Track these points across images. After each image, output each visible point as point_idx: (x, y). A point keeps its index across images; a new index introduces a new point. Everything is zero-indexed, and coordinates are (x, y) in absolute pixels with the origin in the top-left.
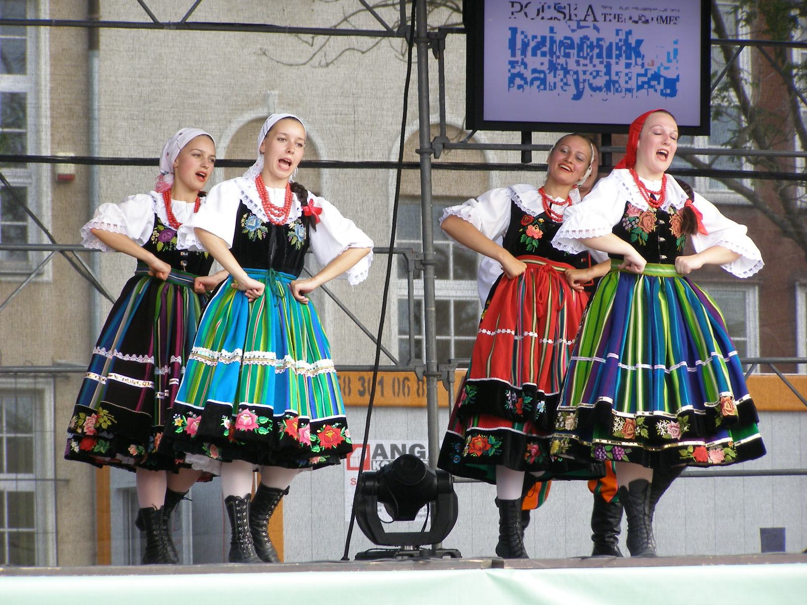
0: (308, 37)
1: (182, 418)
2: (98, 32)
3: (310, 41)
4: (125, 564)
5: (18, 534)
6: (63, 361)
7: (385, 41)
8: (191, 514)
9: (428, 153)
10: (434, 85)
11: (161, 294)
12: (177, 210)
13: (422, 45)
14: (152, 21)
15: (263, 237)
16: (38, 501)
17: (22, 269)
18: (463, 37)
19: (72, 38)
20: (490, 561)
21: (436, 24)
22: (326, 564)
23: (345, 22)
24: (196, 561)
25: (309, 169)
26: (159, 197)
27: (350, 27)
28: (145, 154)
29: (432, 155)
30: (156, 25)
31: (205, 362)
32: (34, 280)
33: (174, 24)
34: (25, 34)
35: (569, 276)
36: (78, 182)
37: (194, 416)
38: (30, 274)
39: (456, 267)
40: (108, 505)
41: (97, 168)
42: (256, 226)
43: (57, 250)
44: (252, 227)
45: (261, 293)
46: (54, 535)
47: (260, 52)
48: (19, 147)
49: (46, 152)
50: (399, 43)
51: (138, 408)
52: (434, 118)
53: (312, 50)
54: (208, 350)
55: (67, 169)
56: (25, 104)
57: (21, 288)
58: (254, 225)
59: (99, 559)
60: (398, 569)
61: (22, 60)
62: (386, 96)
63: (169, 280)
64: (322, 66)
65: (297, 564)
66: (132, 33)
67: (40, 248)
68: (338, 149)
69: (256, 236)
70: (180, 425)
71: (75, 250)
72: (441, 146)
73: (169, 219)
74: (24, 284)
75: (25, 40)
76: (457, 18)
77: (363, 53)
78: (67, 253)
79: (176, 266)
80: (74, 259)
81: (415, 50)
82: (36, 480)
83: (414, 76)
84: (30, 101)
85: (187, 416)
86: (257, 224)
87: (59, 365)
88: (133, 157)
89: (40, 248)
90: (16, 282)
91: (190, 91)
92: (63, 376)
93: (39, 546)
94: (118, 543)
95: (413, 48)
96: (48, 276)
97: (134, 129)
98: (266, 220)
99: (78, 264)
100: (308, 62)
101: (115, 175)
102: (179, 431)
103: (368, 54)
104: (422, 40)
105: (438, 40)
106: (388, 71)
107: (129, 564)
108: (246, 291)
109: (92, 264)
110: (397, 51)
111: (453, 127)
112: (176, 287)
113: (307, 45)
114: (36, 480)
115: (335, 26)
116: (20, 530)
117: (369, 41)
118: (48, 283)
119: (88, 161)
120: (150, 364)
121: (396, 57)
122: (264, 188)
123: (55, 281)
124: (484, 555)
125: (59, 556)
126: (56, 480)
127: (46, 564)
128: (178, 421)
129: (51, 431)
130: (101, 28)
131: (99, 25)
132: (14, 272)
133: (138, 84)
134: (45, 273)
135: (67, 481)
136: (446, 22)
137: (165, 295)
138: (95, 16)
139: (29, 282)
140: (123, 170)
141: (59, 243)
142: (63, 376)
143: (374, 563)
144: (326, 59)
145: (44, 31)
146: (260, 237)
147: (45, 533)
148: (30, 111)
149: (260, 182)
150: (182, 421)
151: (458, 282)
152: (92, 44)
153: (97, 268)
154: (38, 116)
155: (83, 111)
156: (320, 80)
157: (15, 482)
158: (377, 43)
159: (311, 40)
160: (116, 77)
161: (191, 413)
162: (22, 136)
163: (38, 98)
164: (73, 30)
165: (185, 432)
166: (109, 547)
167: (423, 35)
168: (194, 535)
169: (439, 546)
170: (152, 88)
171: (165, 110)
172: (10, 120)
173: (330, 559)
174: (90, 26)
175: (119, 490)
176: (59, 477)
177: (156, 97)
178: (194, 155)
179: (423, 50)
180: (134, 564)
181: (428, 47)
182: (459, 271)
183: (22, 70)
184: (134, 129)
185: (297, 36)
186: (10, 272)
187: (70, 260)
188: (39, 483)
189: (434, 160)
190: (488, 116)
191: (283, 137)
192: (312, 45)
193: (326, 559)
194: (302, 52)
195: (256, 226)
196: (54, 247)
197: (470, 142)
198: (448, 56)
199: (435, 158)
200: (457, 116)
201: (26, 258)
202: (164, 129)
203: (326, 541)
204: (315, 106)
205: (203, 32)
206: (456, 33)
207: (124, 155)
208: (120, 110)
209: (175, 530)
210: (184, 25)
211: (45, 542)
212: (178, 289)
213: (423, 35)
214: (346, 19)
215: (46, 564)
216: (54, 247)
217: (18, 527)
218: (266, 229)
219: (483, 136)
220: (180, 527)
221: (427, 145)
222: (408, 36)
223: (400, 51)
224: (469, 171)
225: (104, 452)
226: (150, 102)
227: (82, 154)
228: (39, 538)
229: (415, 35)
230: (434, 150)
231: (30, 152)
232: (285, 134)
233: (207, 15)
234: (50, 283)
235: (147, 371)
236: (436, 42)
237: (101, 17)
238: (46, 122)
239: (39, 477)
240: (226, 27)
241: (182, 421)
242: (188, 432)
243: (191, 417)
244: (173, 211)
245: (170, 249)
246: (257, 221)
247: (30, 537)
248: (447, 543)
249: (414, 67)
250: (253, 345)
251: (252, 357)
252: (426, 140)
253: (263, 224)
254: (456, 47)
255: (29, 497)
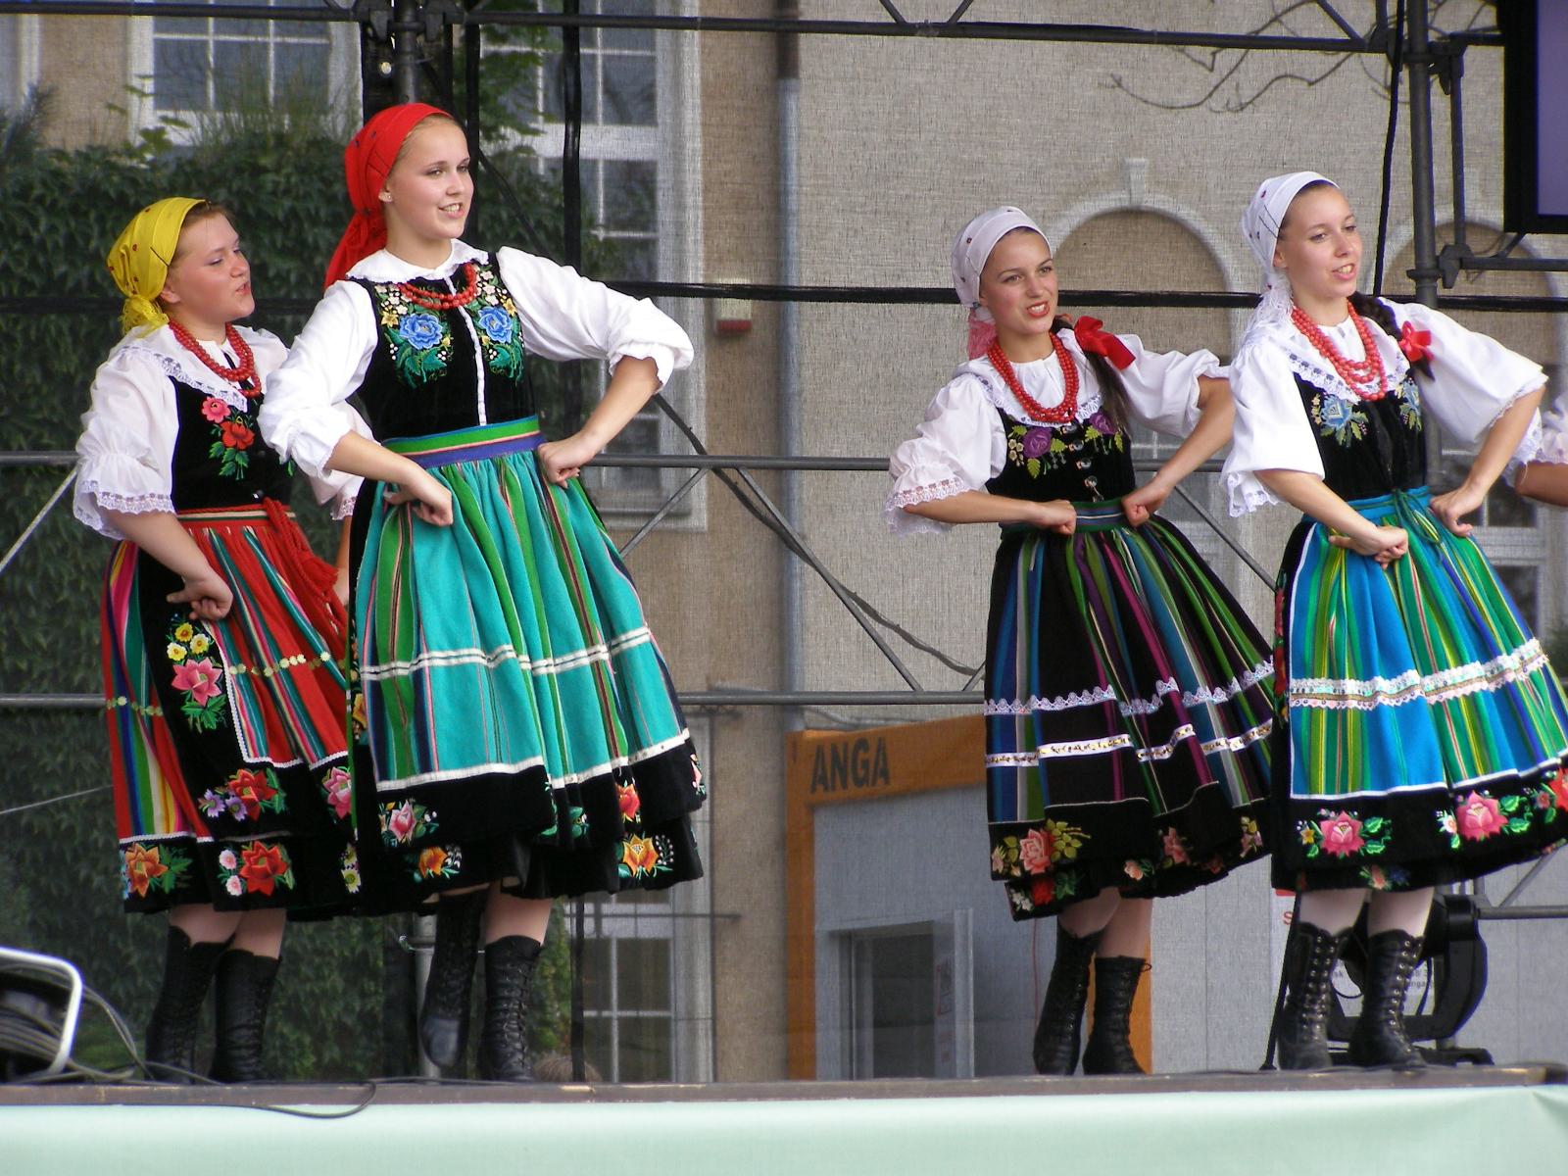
0: (1203, 53)
1: (1311, 827)
2: (796, 41)
3: (1208, 60)
4: (843, 1077)
5: (637, 1020)
6: (728, 684)
7: (1355, 62)
8: (971, 979)
9: (1429, 277)
10: (1442, 145)
11: (1075, 558)
12: (1035, 383)
13: (1418, 66)
14: (892, 20)
15: (1362, 434)
16: (677, 958)
17: (636, 505)
18: (1497, 53)
19: (748, 52)
20: (1542, 1071)
21: (1449, 30)
22: (1224, 1076)
23: (1276, 24)
24: (981, 1072)
25: (1196, 309)
26: (982, 366)
27: (1284, 33)
28: (878, 280)
29: (1439, 282)
30: (900, 28)
31: (1323, 706)
32: (660, 526)
33: (936, 25)
34: (652, 46)
35: (1446, 514)
36: (760, 335)
37: (1333, 814)
38: (652, 515)
39: (1497, 502)
40: (812, 962)
41: (794, 306)
42: (1345, 416)
43: (708, 466)
44: (1340, 421)
45: (1404, 550)
46: (710, 1022)
47: (1110, 81)
48: (644, 271)
49: (695, 276)
50: (1378, 63)
51: (1117, 793)
52: (1443, 213)
53: (1214, 78)
54: (1323, 680)
55: (734, 310)
56: (654, 182)
57: (636, 540)
58: (1341, 416)
59: (793, 1068)
60: (1363, 1086)
61: (649, 97)
62: (1346, 167)
63: (1080, 527)
64: (1229, 110)
65: (1168, 1077)
66: (852, 45)
67: (680, 463)
68: (1253, 271)
69: (1350, 435)
70: (1312, 840)
71: (741, 465)
72: (1455, 264)
73: (1026, 409)
74: (643, 533)
75: (653, 59)
76: (1488, 18)
77: (1311, 84)
78: (726, 471)
79: (1077, 494)
80: (742, 486)
81: (1405, 74)
82: (674, 916)
83: (1403, 128)
84: (664, 180)
85: (1320, 819)
86: (1345, 412)
87: (719, 691)
88: (854, 285)
89: (680, 463)
90: (626, 531)
91: (965, 156)
92: (729, 713)
93: (679, 1042)
94: (829, 1038)
95: (1401, 74)
96: (699, 519)
97: (856, 231)
98: (1355, 399)
99: (748, 492)
100: (1202, 102)
101: (818, 320)
102: (1313, 853)
103: (1317, 86)
104: (1417, 54)
105: (1450, 57)
106: (1351, 117)
107: (851, 1078)
108: (1377, 555)
109: (783, 495)
110: (1376, 80)
111: (1484, 228)
112: (1096, 536)
113: (1201, 68)
114: (674, 916)
115: (1257, 32)
116: (643, 1014)
117: (1315, 62)
118: (699, 533)
119: (776, 294)
120: (1110, 701)
121: (1376, 91)
122: (1318, 331)
123: (712, 530)
124: (1532, 1059)
125: (719, 1064)
126: (713, 916)
127: (692, 1078)
128: (1306, 835)
129: (703, 822)
130: (802, 35)
131: (797, 27)
132: (621, 510)
133: (865, 144)
134: (693, 512)
135: (735, 918)
136: (1472, 22)
137: (1083, 560)
138: (790, 11)
139: (651, 530)
140: (835, 311)
141: (711, 453)
142: (729, 713)
143: (1317, 1075)
144: (1238, 95)
145: (693, 39)
146: (1358, 436)
147: (691, 1019)
148: (663, 198)
149: (1301, 319)
150: (1313, 832)
151: (1495, 530)
152: (785, 65)
153: (796, 510)
154: (680, 206)
155: (766, 199)
156: (1221, 137)
157: (632, 921)
158: (1339, 65)
159: (1210, 58)
160: (821, 130)
161: (1324, 812)
162: (648, 246)
163: (678, 171)
164: (752, 39)
165: (1323, 851)
166: (812, 1046)
167: (1420, 48)
168: (977, 1020)
169: (1449, 1043)
170: (892, 151)
171: (917, 194)
172: (625, 215)
173: (1233, 1067)
174: (782, 31)
175: (834, 935)
176: (718, 910)
177: (900, 169)
178: (1006, 281)
179: (1421, 76)
180: (860, 1076)
181: (1431, 72)
182: (1502, 510)
183: (648, 118)
184: (856, 231)
185: (1182, 51)
186: (614, 510)
187: (734, 487)
188: (680, 921)
189: (1442, 292)
190: (1548, 205)
191: (1320, 231)
192: (1212, 70)
193: (1224, 1067)
194: (1185, 81)
195: (1345, 416)
196: (701, 461)
197: (1513, 255)
198: (1469, 88)
199: (1445, 286)
200: (1487, 206)
201: (657, 486)
202: (914, 231)
203: (1226, 1033)
204: (1211, 186)
205: (991, 41)
206: (1483, 44)
207: (838, 281)
208: (828, 194)
209: (940, 1013)
210: (954, 29)
211: (693, 1033)
212: (1104, 541)
213: (1420, 48)
214: (1276, 19)
215: (692, 1078)
216: (701, 461)
217: (637, 1008)
218: (1363, 415)
219: (1541, 245)
220: (951, 1010)
221: (1428, 263)
222: (1391, 48)
223: (1382, 80)
224: (1508, 314)
225: (1072, 893)
226: (887, 180)
227: (763, 280)
228: (680, 1029)
229: (1405, 48)
230: (1443, 271)
231: (665, 276)
232: (1321, 226)
233: (998, 9)
234: (703, 534)
235: (1109, 716)
236: (1444, 61)
237: (801, 14)
238: (695, 217)
239: (681, 910)
240: (1037, 33)
241: (1313, 832)
242: (1330, 850)
243: (1326, 818)
244: (1028, 389)
245: (1055, 467)
246: (1342, 405)
247: (663, 1028)
248: (1466, 1037)
249: (1404, 112)
250: (1433, 659)
251: (1441, 684)
252: (1427, 250)
253: (1355, 409)
254: (1484, 72)
255: (659, 949)
